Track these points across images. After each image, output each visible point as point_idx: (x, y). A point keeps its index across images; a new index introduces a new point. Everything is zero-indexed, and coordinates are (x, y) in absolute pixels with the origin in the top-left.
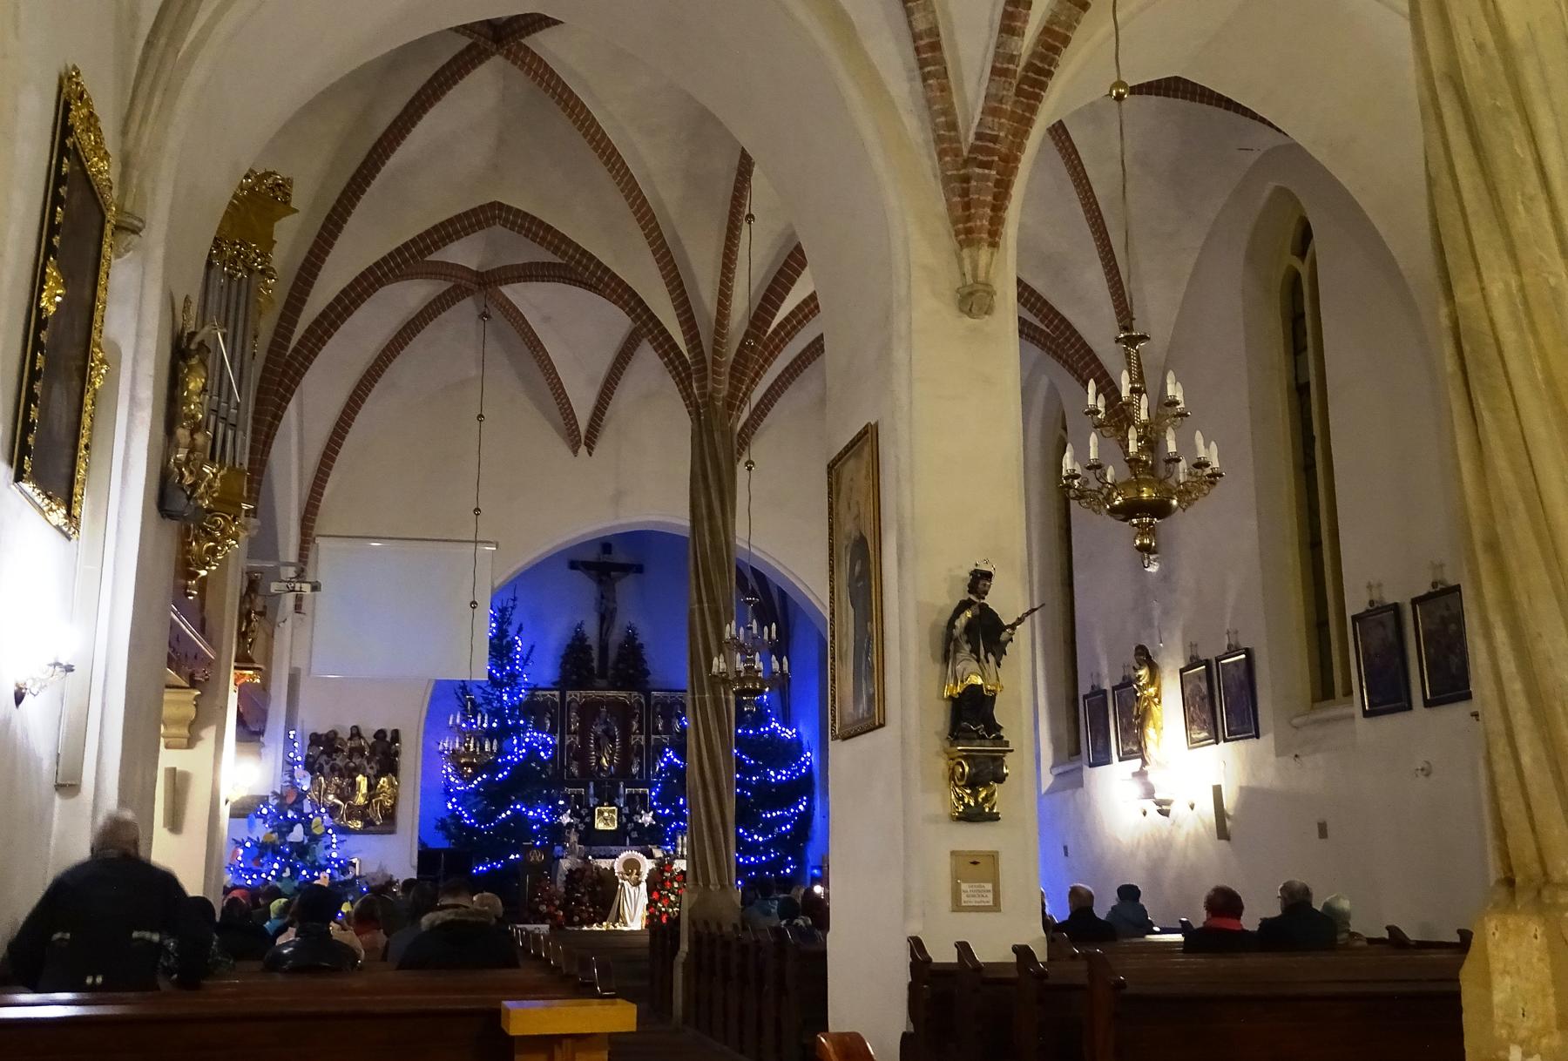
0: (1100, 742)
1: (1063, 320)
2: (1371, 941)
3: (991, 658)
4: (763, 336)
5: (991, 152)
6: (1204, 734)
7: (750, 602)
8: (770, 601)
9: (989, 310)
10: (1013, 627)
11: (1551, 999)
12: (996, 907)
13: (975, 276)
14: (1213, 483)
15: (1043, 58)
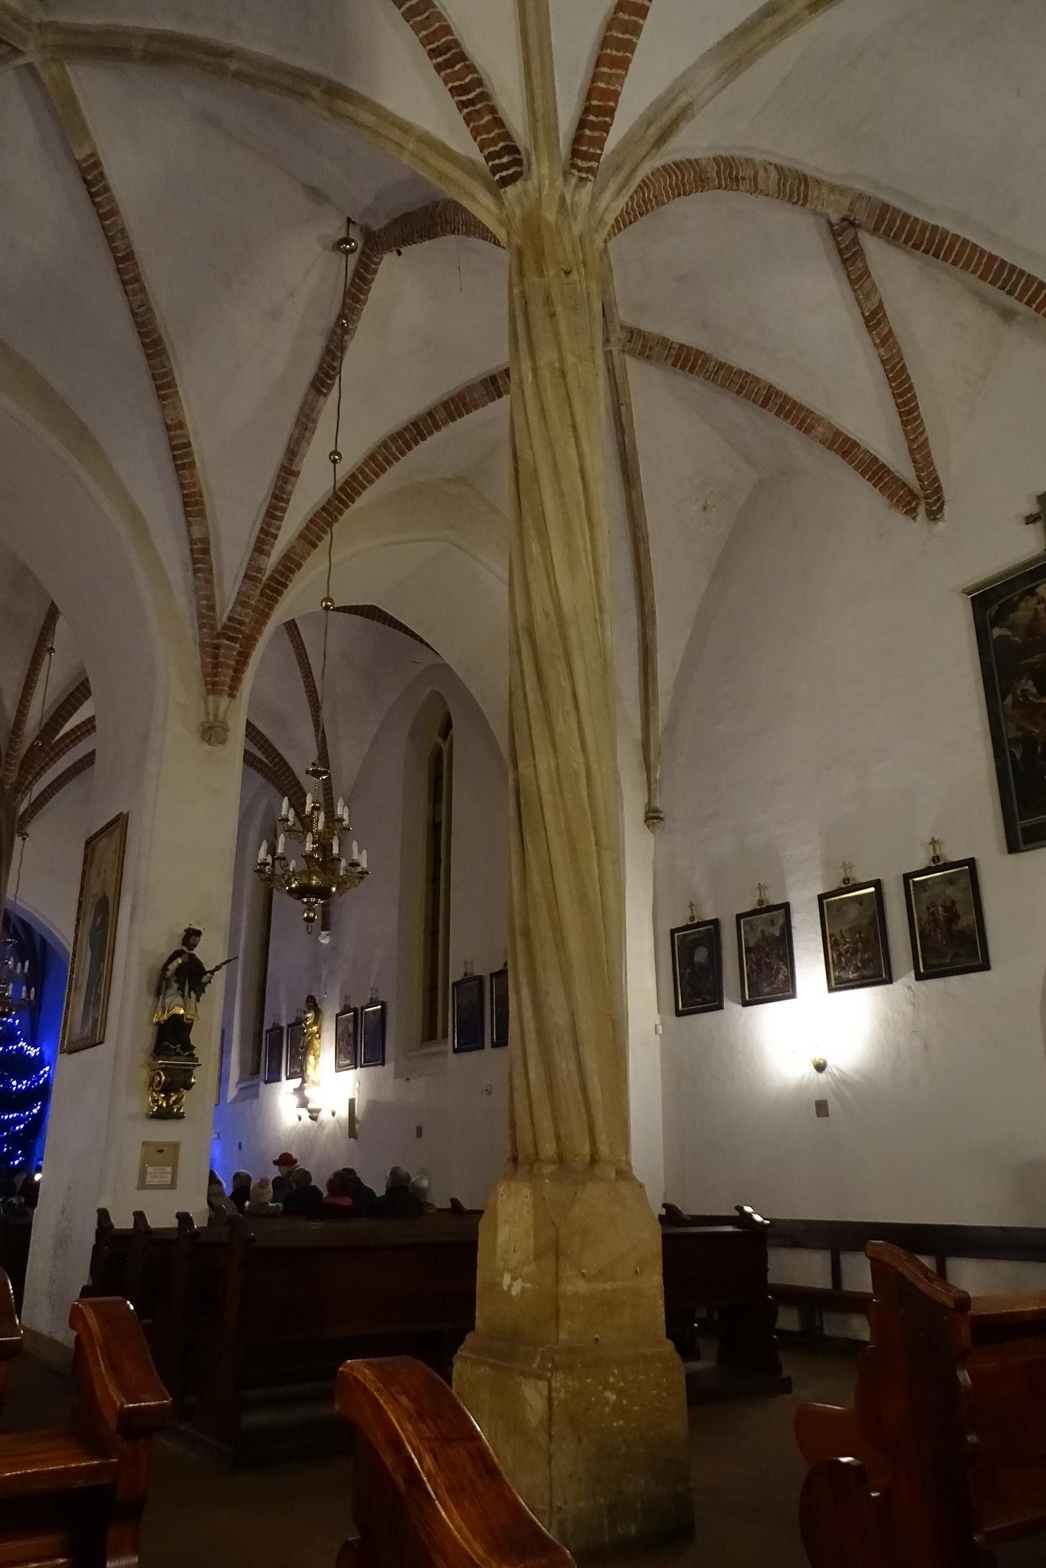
0: (274, 1066)
1: (282, 759)
2: (439, 1210)
3: (193, 995)
4: (49, 743)
5: (236, 630)
6: (348, 1062)
7: (9, 943)
8: (30, 943)
9: (223, 742)
10: (212, 972)
11: (532, 1240)
12: (172, 1185)
13: (216, 715)
14: (362, 878)
15: (282, 574)
